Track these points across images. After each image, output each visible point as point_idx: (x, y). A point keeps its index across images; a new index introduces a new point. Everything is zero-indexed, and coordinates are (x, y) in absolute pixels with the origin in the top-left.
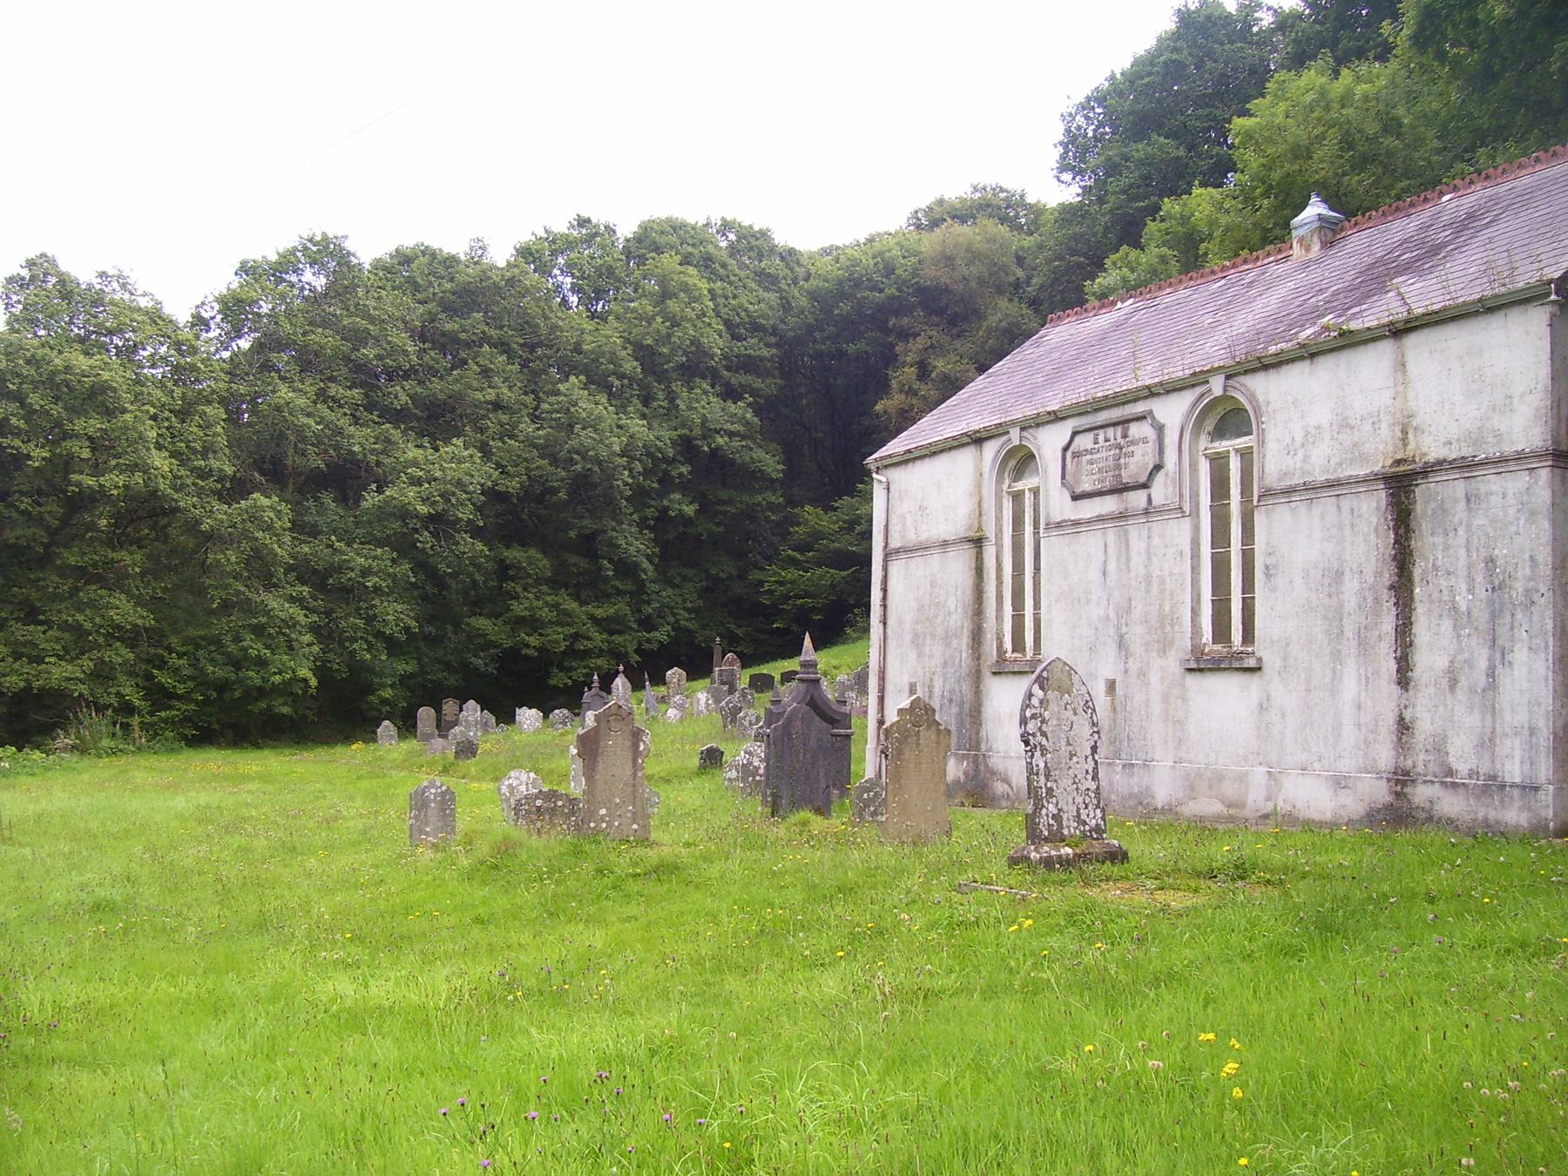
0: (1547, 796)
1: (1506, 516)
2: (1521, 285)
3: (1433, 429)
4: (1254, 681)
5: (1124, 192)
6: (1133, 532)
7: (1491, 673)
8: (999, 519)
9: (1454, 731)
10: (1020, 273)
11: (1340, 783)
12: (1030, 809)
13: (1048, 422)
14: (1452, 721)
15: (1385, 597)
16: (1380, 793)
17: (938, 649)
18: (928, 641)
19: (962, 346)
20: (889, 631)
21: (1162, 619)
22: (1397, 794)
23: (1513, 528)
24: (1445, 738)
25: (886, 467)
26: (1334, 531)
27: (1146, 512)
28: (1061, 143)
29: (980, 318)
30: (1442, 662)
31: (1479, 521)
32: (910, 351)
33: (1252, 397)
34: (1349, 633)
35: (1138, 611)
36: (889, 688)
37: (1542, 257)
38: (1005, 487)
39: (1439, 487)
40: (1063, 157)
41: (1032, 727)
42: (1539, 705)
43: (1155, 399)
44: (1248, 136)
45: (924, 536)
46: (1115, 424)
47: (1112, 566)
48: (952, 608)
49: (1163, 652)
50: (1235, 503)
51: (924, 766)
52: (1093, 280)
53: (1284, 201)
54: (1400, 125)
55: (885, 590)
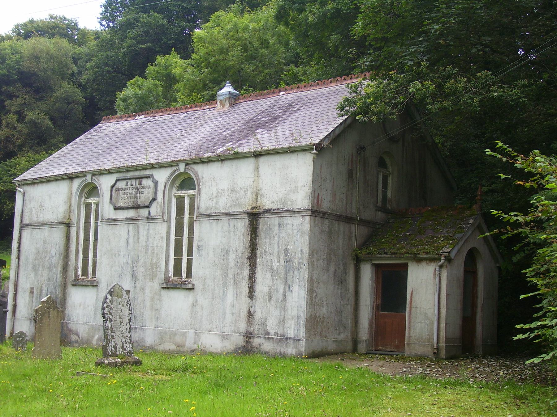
0: (303, 343)
1: (293, 233)
2: (303, 144)
3: (268, 196)
4: (191, 294)
5: (134, 38)
6: (141, 227)
7: (284, 295)
8: (79, 215)
9: (269, 316)
10: (75, 69)
11: (224, 337)
12: (104, 343)
13: (105, 174)
14: (269, 313)
15: (246, 262)
16: (240, 341)
17: (45, 273)
18: (41, 269)
19: (43, 105)
20: (21, 263)
21: (152, 265)
22: (247, 342)
23: (295, 238)
24: (266, 320)
25: (23, 185)
26: (227, 233)
27: (148, 219)
28: (104, 5)
29: (52, 91)
30: (266, 289)
31: (283, 234)
32: (14, 105)
33: (196, 174)
34: (230, 276)
35: (141, 261)
36: (20, 290)
37: (313, 132)
38: (82, 200)
39: (269, 219)
40: (104, 13)
41: (106, 311)
42: (301, 307)
43: (154, 170)
44: (201, 39)
45: (41, 219)
46: (136, 178)
47: (131, 241)
48: (54, 254)
49: (152, 280)
50: (186, 219)
51: (51, 326)
52: (121, 92)
53: (214, 70)
54: (268, 43)
55: (19, 243)
